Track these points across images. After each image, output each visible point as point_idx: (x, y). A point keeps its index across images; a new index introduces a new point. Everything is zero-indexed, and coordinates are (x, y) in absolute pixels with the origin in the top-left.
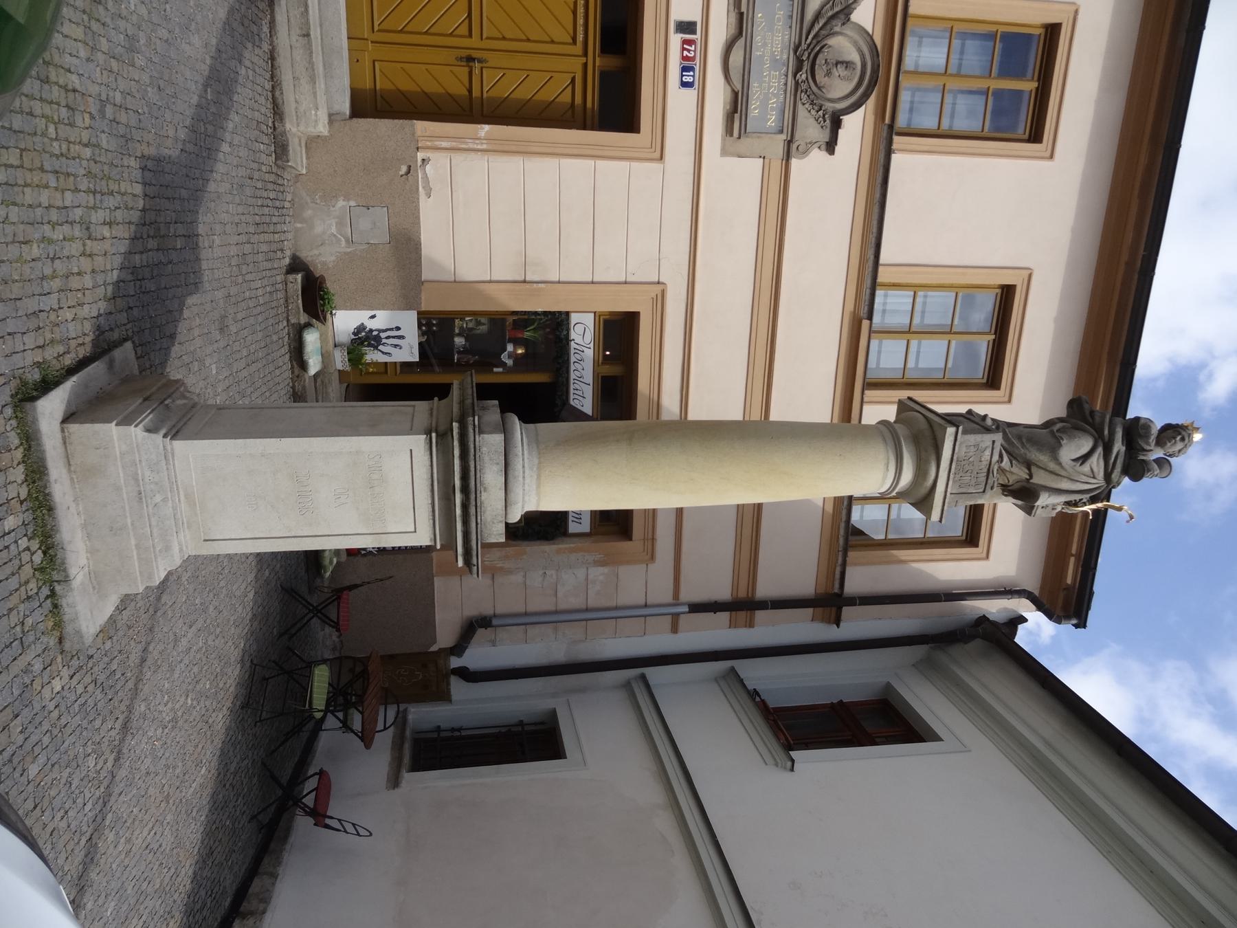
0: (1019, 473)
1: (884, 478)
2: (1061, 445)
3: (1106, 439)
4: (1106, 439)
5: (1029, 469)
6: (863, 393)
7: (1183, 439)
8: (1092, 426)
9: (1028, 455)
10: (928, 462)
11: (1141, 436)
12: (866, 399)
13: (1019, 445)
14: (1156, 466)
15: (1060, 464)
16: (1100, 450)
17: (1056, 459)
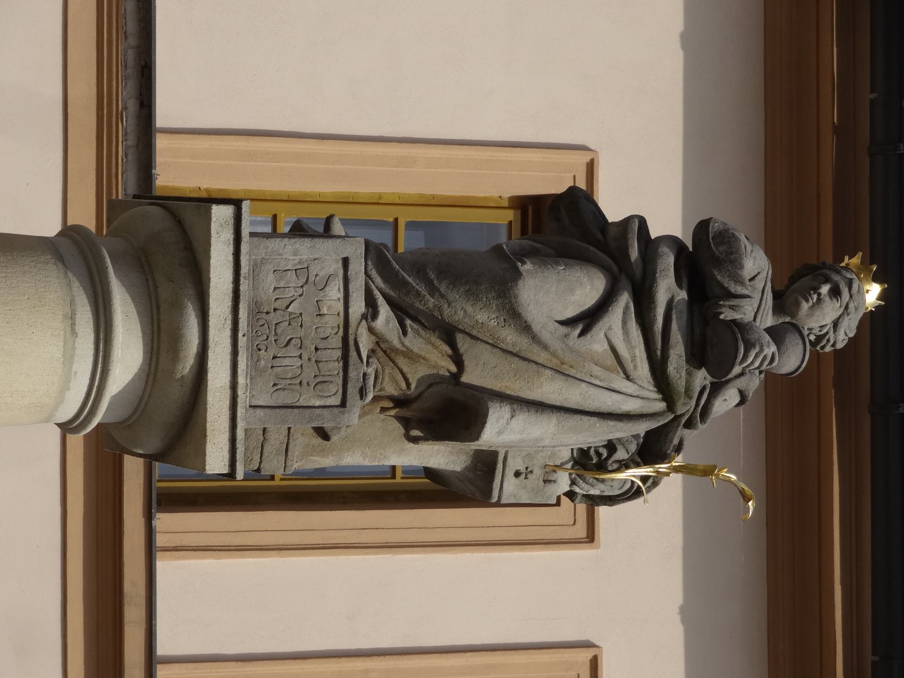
0: (434, 358)
1: (69, 357)
2: (518, 275)
3: (638, 273)
4: (638, 273)
5: (452, 344)
6: (149, 518)
7: (835, 293)
8: (604, 247)
9: (447, 312)
10: (177, 308)
11: (718, 262)
12: (161, 540)
13: (422, 289)
14: (767, 338)
15: (526, 328)
16: (624, 299)
17: (513, 315)
